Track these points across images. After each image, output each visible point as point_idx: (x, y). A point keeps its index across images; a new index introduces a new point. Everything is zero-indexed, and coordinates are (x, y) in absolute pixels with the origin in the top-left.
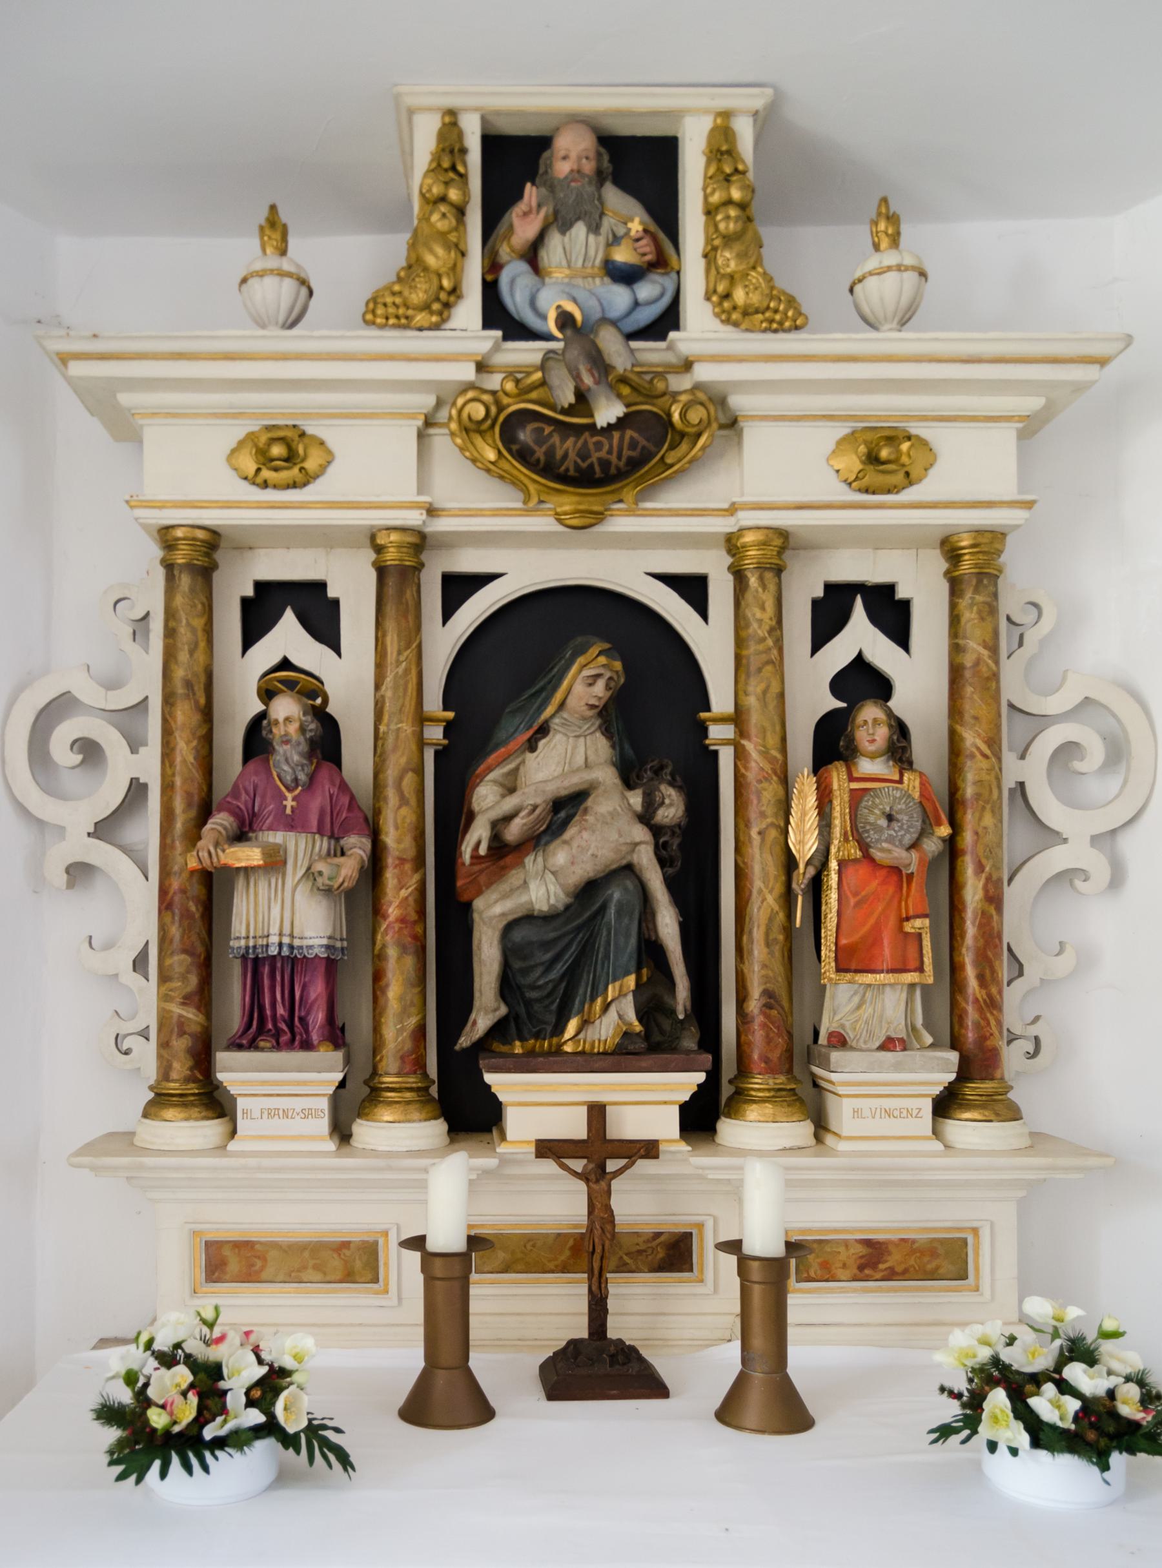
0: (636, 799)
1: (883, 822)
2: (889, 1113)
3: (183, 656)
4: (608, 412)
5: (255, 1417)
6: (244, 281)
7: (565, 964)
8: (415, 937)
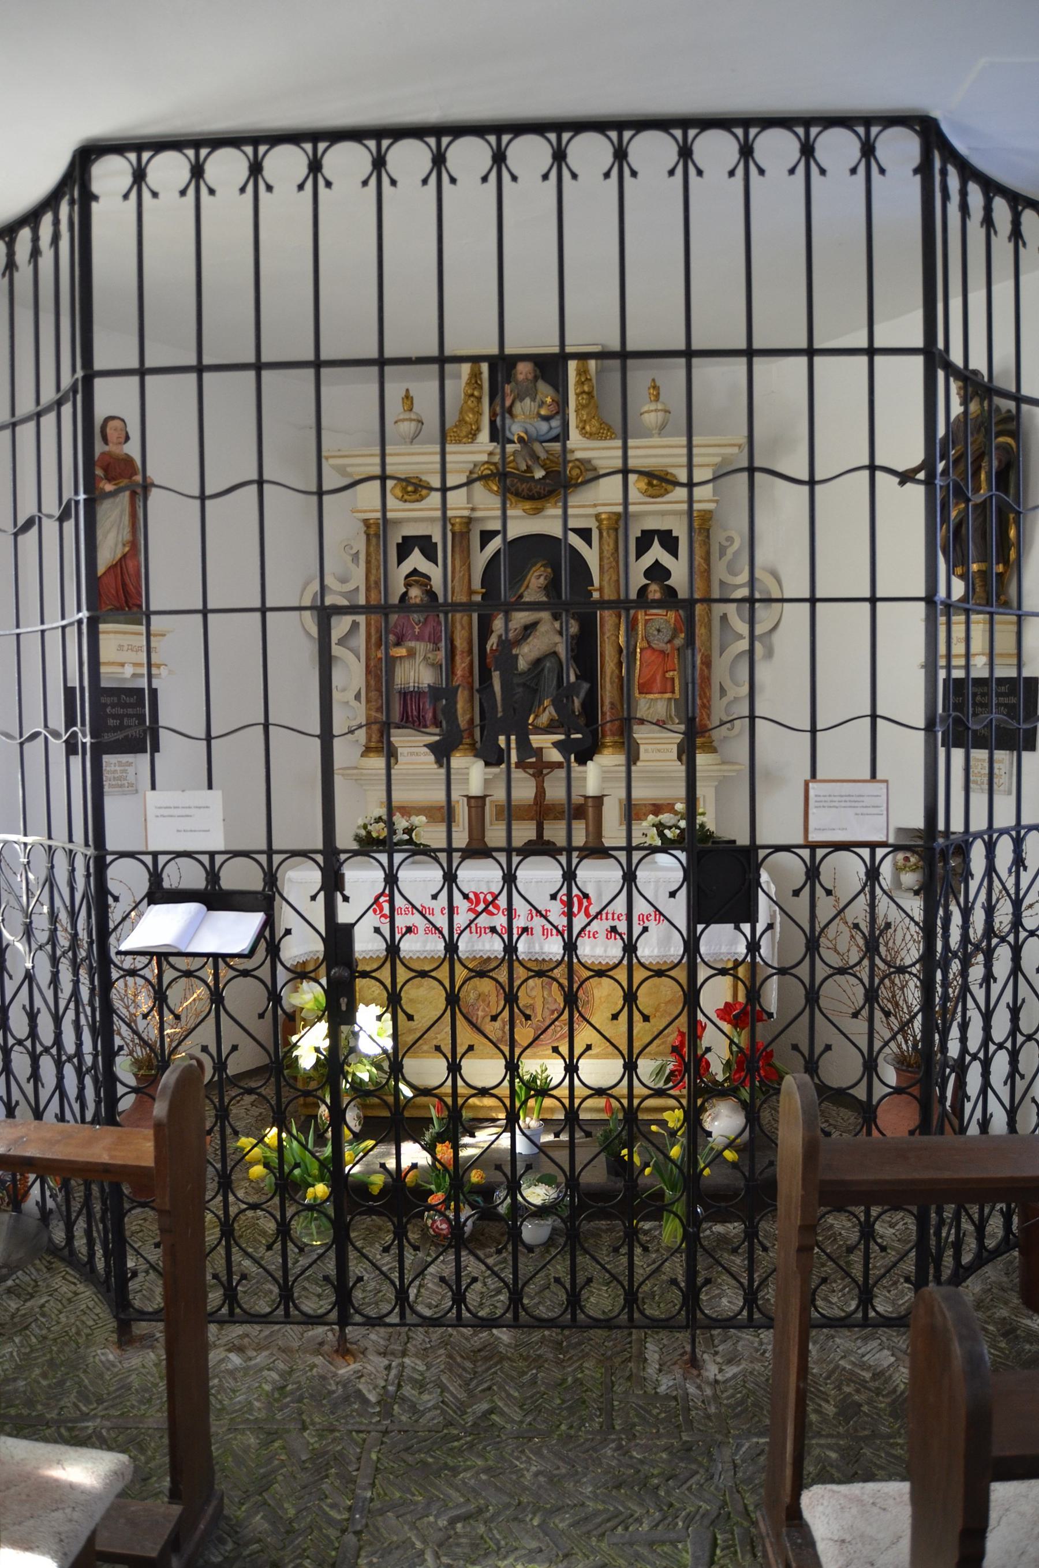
0: (557, 625)
1: (656, 633)
2: (659, 751)
4: (539, 474)
5: (406, 837)
6: (396, 422)
7: (720, 771)
8: (468, 683)
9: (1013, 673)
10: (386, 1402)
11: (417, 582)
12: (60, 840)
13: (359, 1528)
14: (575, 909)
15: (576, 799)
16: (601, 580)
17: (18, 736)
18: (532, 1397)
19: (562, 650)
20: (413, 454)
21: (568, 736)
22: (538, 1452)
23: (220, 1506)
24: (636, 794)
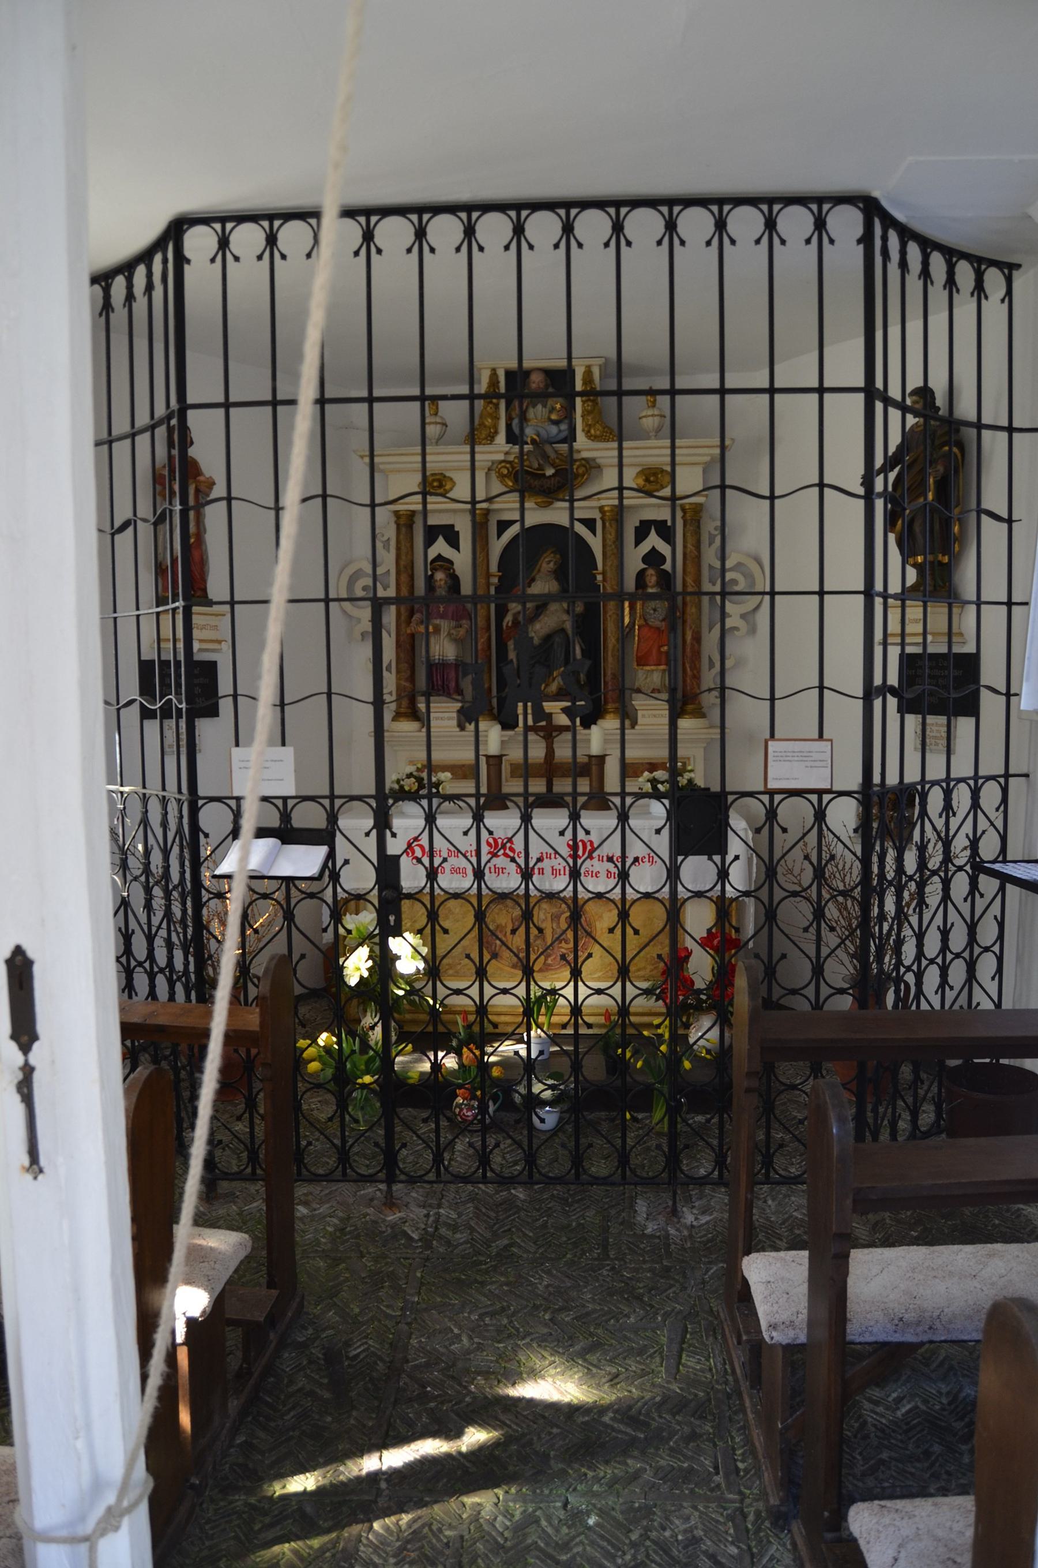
2: (655, 716)
3: (403, 557)
4: (550, 472)
9: (943, 649)
10: (426, 1241)
11: (441, 566)
12: (154, 787)
13: (409, 1320)
14: (580, 853)
15: (581, 759)
16: (604, 565)
17: (115, 703)
18: (543, 1235)
19: (568, 626)
20: (438, 454)
21: (574, 704)
22: (548, 1273)
23: (301, 1305)
24: (629, 754)
